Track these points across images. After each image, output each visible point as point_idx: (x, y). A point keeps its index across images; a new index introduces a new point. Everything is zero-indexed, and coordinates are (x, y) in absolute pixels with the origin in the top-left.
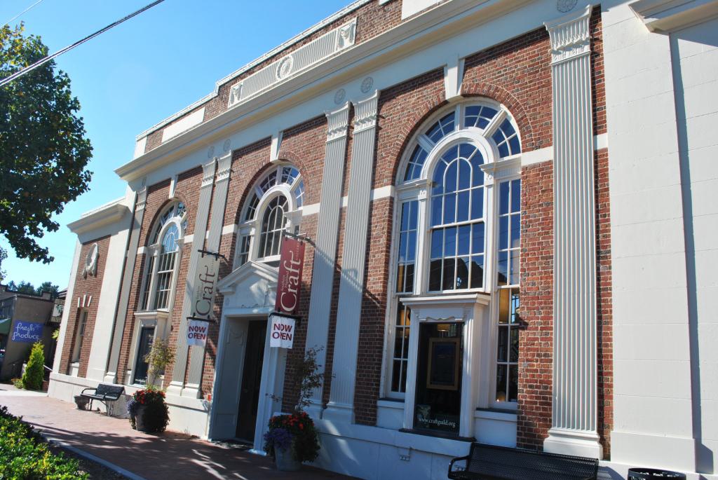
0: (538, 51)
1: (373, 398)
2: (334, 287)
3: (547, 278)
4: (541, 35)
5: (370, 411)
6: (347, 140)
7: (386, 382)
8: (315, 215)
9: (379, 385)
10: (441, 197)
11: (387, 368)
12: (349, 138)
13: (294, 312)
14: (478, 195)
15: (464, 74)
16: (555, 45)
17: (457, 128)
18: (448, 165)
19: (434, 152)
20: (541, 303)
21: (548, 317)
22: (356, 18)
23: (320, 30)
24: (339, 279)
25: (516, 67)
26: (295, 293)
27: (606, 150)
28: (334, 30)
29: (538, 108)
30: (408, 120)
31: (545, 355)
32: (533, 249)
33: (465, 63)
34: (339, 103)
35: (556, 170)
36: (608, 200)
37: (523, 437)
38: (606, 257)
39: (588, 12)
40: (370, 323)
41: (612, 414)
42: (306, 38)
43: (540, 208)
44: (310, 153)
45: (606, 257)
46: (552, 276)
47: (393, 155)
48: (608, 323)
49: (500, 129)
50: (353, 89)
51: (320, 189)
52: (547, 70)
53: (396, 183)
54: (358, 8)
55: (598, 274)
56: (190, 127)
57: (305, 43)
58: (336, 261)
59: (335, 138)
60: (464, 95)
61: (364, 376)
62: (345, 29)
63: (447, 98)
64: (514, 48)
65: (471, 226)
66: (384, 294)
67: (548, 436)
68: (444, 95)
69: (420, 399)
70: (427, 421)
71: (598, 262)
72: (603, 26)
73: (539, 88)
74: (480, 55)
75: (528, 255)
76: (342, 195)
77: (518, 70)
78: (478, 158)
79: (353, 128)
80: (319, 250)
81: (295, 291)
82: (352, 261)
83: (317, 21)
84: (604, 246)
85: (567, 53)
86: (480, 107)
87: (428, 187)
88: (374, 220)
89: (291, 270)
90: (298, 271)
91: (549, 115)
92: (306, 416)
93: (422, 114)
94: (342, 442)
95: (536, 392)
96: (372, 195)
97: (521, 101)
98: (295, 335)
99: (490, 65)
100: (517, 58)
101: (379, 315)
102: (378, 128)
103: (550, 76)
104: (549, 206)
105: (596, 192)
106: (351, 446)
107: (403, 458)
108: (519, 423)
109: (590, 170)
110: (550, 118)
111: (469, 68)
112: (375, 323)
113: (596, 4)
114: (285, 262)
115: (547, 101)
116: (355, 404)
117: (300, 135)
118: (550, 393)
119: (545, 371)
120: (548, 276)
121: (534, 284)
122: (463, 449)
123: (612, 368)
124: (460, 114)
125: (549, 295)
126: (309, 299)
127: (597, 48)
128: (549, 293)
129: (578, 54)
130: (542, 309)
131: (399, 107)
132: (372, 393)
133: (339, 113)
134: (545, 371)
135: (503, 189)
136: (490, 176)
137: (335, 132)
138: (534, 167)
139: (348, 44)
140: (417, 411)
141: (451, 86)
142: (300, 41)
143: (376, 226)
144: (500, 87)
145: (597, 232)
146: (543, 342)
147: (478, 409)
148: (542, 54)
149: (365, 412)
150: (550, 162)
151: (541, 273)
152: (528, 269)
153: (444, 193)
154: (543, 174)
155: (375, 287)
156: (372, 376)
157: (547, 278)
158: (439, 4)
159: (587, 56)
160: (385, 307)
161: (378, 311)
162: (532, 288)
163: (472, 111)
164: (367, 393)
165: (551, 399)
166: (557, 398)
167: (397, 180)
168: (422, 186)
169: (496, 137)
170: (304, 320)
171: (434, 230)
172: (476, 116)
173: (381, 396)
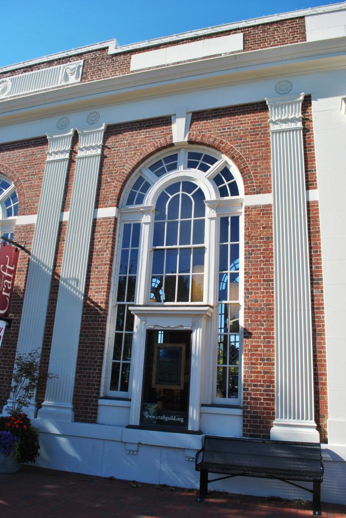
0: (258, 119)
1: (94, 397)
2: (51, 293)
3: (268, 297)
4: (262, 107)
5: (91, 409)
6: (101, 158)
7: (106, 383)
8: (31, 225)
9: (99, 385)
10: (165, 223)
11: (106, 370)
12: (71, 161)
13: (6, 314)
14: (200, 226)
15: (191, 125)
16: (273, 117)
17: (181, 168)
18: (171, 197)
19: (158, 185)
20: (263, 317)
21: (270, 329)
22: (82, 61)
23: (43, 63)
24: (58, 286)
25: (239, 127)
26: (7, 296)
27: (317, 202)
28: (59, 66)
29: (258, 162)
30: (135, 154)
31: (268, 359)
32: (256, 273)
33: (192, 116)
34: (62, 128)
35: (275, 212)
36: (319, 240)
37: (248, 428)
38: (319, 284)
39: (302, 98)
40: (91, 328)
41: (326, 406)
42: (27, 67)
43: (262, 241)
44: (26, 168)
45: (319, 284)
46: (273, 296)
47: (118, 181)
48: (320, 334)
49: (10, 198)
50: (77, 120)
51: (38, 202)
52: (266, 134)
53: (120, 206)
54: (85, 53)
55: (312, 296)
56: (166, 63)
57: (25, 72)
58: (54, 269)
59: (56, 159)
60: (190, 142)
61: (84, 376)
62: (71, 67)
63: (174, 141)
64: (237, 112)
65: (166, 251)
66: (107, 303)
67: (272, 427)
68: (171, 138)
69: (148, 395)
70: (154, 417)
71: (312, 287)
72: (312, 110)
73: (259, 147)
74: (207, 112)
75: (251, 277)
76: (63, 210)
77: (241, 130)
78: (200, 195)
79: (77, 153)
80: (35, 258)
81: (8, 295)
82: (73, 270)
83: (41, 56)
84: (317, 275)
85: (284, 124)
86: (202, 154)
87: (151, 213)
88: (97, 235)
89: (6, 274)
90: (11, 276)
91: (268, 169)
92: (25, 416)
93: (149, 151)
94: (63, 441)
95: (260, 390)
96: (95, 213)
97: (244, 155)
98: (4, 336)
99: (215, 122)
100: (239, 121)
101: (102, 321)
102: (103, 157)
103: (269, 139)
104: (269, 239)
105: (309, 233)
106: (74, 445)
107: (131, 453)
108: (244, 416)
109: (304, 216)
110: (269, 172)
111: (196, 121)
112: (98, 328)
113: (308, 93)
114: (2, 266)
115: (267, 158)
116: (73, 404)
117: (16, 151)
118: (273, 391)
119: (268, 373)
120: (270, 295)
121: (257, 301)
122: (194, 442)
123: (325, 370)
124: (183, 157)
125: (270, 311)
126: (22, 303)
127: (308, 125)
128: (270, 309)
129: (292, 127)
130: (265, 321)
131: (126, 142)
132: (93, 393)
133: (64, 137)
134: (268, 373)
135: (223, 222)
136: (213, 211)
137: (56, 153)
138: (255, 207)
139: (73, 80)
140: (143, 408)
141: (179, 132)
142: (20, 69)
143: (100, 241)
144: (224, 140)
145: (311, 264)
146: (265, 349)
147: (203, 405)
148: (261, 121)
149: (85, 408)
150: (270, 206)
151: (263, 293)
152: (251, 289)
153: (167, 220)
154: (263, 214)
155: (98, 297)
156: (93, 377)
157: (268, 297)
158: (167, 65)
159: (99, 156)
160: (107, 314)
161: (101, 317)
162: (255, 304)
163: (191, 155)
164: (88, 392)
165: (273, 395)
166: (279, 395)
167: (121, 203)
168: (146, 211)
169: (217, 180)
170: (15, 323)
171: (155, 250)
172: (199, 161)
173: (102, 395)
